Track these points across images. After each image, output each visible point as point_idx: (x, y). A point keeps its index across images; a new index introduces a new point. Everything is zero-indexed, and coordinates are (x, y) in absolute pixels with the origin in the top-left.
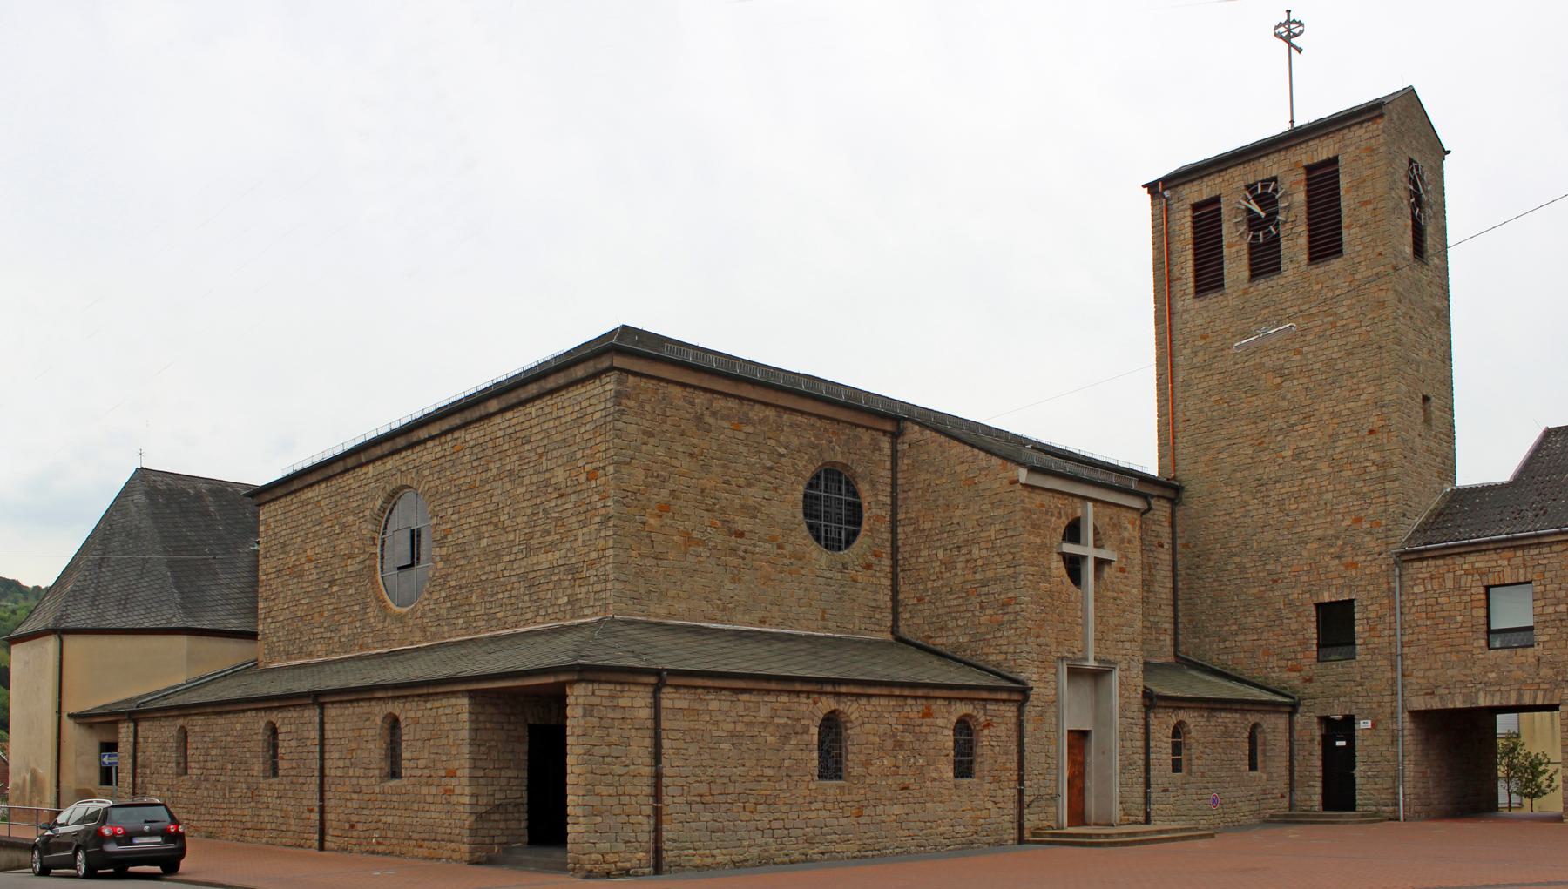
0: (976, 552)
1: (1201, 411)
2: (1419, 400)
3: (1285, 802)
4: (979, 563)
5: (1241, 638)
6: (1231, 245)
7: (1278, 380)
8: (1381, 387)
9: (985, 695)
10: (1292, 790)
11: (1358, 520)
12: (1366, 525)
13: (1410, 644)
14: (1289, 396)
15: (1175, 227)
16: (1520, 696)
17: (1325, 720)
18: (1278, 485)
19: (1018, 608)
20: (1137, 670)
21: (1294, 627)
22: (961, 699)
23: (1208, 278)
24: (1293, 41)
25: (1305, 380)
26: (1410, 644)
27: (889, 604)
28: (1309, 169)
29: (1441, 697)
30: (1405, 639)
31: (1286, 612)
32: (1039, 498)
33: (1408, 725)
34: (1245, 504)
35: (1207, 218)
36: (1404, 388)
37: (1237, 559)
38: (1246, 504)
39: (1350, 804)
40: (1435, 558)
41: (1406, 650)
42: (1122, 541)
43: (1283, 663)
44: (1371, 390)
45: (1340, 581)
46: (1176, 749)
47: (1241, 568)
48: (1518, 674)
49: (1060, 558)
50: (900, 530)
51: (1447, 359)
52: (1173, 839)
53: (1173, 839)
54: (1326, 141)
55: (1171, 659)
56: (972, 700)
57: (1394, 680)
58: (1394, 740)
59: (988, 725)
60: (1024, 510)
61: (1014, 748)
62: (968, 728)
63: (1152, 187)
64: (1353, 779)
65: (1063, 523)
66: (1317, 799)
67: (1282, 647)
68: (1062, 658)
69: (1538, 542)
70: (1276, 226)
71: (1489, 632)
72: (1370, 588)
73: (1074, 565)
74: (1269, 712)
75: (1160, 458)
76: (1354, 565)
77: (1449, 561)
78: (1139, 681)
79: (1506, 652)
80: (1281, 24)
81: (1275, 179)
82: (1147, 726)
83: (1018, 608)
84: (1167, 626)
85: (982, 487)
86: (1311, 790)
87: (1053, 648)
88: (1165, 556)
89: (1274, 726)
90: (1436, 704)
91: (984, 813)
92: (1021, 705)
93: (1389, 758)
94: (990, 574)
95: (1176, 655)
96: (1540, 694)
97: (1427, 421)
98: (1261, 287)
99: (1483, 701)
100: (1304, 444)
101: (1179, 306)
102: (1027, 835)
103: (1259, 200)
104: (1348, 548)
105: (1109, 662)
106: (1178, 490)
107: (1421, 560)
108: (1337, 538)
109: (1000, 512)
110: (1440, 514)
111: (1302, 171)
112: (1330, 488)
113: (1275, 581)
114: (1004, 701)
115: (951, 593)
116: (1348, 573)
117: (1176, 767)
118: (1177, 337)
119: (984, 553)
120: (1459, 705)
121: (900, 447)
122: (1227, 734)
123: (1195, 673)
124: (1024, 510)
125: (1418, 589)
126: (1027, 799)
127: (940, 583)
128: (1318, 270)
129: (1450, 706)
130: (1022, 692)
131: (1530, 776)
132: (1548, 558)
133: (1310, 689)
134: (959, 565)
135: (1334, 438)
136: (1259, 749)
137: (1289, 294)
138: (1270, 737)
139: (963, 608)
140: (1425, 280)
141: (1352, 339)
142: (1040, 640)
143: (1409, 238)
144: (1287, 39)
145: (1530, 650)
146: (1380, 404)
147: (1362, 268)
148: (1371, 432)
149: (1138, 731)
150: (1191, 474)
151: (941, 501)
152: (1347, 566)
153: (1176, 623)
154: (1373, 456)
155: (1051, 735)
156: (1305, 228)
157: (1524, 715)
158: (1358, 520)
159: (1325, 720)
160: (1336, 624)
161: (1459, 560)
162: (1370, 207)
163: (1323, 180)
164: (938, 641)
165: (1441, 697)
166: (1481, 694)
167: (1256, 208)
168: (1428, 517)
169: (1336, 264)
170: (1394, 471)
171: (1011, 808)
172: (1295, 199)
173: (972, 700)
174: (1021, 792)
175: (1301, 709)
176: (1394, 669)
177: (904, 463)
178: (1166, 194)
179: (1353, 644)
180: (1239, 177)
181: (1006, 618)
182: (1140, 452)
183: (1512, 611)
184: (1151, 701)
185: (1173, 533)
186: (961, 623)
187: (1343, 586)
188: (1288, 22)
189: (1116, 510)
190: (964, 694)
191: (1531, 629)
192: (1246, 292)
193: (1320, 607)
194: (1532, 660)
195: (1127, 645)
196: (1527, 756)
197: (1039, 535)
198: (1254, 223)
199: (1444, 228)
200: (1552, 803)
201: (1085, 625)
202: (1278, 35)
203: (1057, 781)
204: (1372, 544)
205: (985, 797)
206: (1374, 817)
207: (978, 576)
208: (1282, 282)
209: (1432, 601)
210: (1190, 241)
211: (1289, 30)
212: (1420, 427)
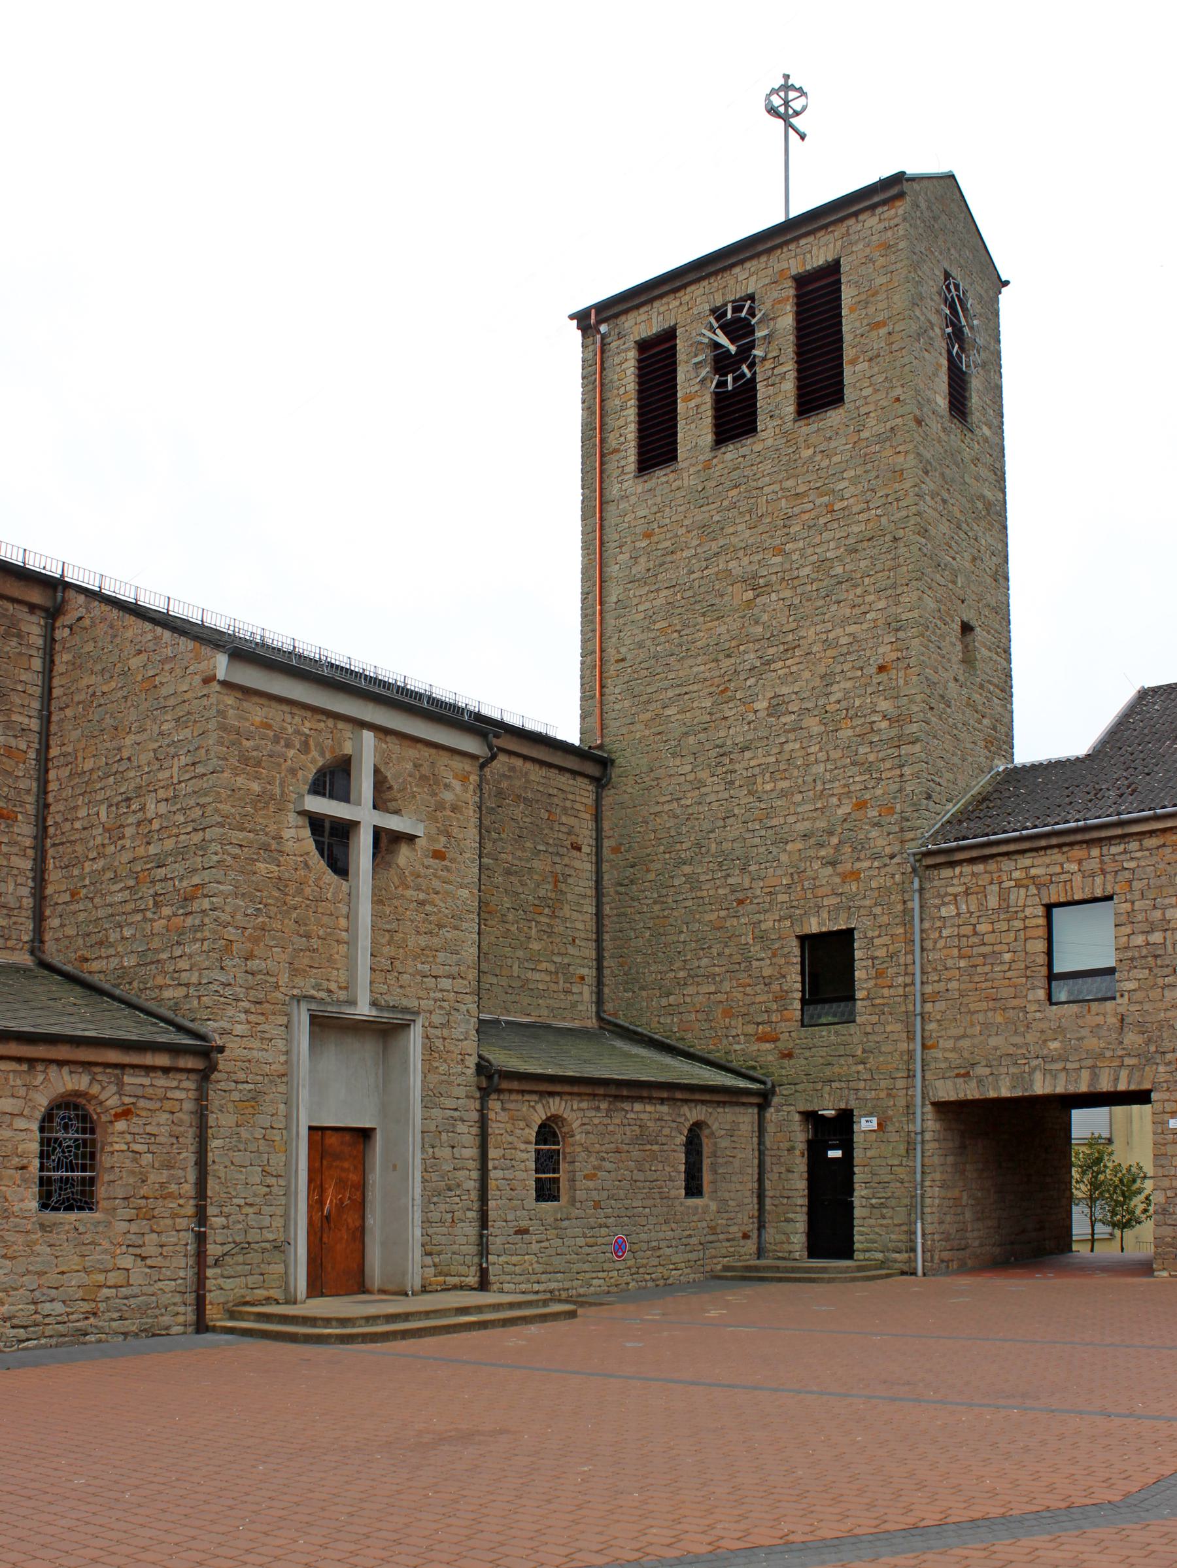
0: (151, 807)
1: (640, 645)
2: (957, 627)
3: (751, 1246)
4: (156, 825)
5: (691, 990)
6: (688, 398)
7: (750, 594)
8: (896, 600)
9: (114, 1056)
10: (761, 1227)
11: (861, 805)
12: (873, 813)
13: (935, 997)
14: (765, 617)
15: (612, 376)
16: (1094, 1077)
17: (810, 1117)
18: (748, 755)
19: (206, 904)
20: (464, 1028)
21: (767, 972)
22: (61, 1063)
23: (657, 447)
24: (793, 121)
25: (787, 593)
26: (935, 997)
27: (28, 902)
28: (801, 281)
29: (980, 1081)
30: (928, 989)
31: (756, 950)
32: (258, 713)
33: (930, 1124)
34: (699, 784)
35: (657, 359)
36: (931, 604)
37: (687, 869)
38: (702, 784)
39: (845, 1250)
40: (972, 861)
41: (929, 1007)
42: (440, 806)
43: (751, 1029)
44: (881, 604)
45: (833, 900)
46: (547, 1162)
47: (693, 882)
48: (1092, 1043)
49: (303, 821)
50: (52, 775)
51: (1001, 576)
52: (483, 1325)
53: (483, 1325)
54: (824, 238)
55: (592, 1023)
56: (87, 1065)
57: (911, 1054)
58: (910, 1149)
59: (126, 1113)
60: (223, 728)
61: (188, 1157)
62: (85, 1118)
63: (584, 320)
64: (850, 1207)
65: (314, 762)
66: (798, 1239)
67: (746, 1003)
68: (298, 999)
69: (1121, 833)
70: (751, 366)
71: (1051, 977)
72: (878, 910)
73: (333, 839)
74: (723, 1104)
75: (583, 717)
76: (855, 875)
77: (992, 866)
78: (470, 1046)
79: (1074, 1008)
80: (774, 91)
81: (752, 297)
82: (483, 1123)
83: (206, 904)
84: (585, 971)
85: (164, 691)
86: (788, 1227)
87: (284, 979)
88: (586, 866)
89: (730, 1128)
90: (970, 1091)
91: (113, 1278)
92: (205, 1076)
93: (906, 1179)
94: (169, 844)
95: (600, 1018)
96: (1124, 1074)
97: (968, 660)
98: (729, 456)
99: (1040, 1086)
100: (785, 690)
101: (614, 491)
102: (213, 1314)
103: (726, 328)
104: (847, 849)
105: (406, 1010)
106: (605, 763)
107: (952, 864)
108: (831, 833)
109: (187, 733)
110: (985, 799)
111: (789, 283)
112: (822, 756)
113: (741, 902)
114: (166, 1070)
115: (115, 879)
116: (846, 888)
117: (546, 1191)
118: (612, 536)
119: (163, 808)
120: (1005, 1093)
121: (58, 635)
122: (643, 1138)
123: (619, 1044)
124: (223, 728)
125: (948, 911)
126: (213, 1250)
127: (100, 864)
128: (806, 429)
129: (992, 1094)
130: (203, 1057)
131: (1118, 1197)
132: (1137, 857)
133: (791, 1068)
134: (129, 831)
135: (828, 679)
136: (706, 1162)
137: (767, 467)
138: (724, 1143)
139: (130, 907)
140: (967, 454)
141: (856, 529)
142: (253, 965)
143: (942, 383)
144: (785, 118)
145: (1109, 1005)
146: (895, 626)
147: (871, 422)
148: (882, 669)
149: (467, 1133)
150: (629, 747)
151: (109, 721)
152: (845, 877)
153: (600, 969)
154: (884, 705)
155: (276, 1136)
156: (796, 369)
157: (1119, 1110)
158: (861, 805)
159: (810, 1117)
160: (828, 967)
161: (1007, 864)
162: (883, 331)
163: (819, 297)
164: (95, 966)
165: (980, 1081)
166: (1038, 1076)
167: (723, 340)
168: (966, 806)
169: (834, 417)
170: (914, 728)
171: (181, 1267)
172: (779, 326)
173: (87, 1065)
174: (201, 1238)
175: (776, 1100)
176: (911, 1038)
177: (63, 659)
178: (603, 328)
179: (852, 998)
180: (703, 297)
181: (189, 921)
182: (554, 708)
183: (1086, 942)
184: (491, 1081)
185: (599, 830)
186: (127, 932)
187: (838, 908)
188: (786, 87)
189: (426, 752)
190: (63, 1052)
191: (1111, 971)
192: (707, 466)
193: (804, 939)
194: (1112, 1020)
195: (446, 983)
196: (1117, 1169)
197: (257, 778)
198: (722, 363)
199: (999, 388)
200: (1142, 1240)
201: (352, 943)
202: (772, 111)
203: (286, 1216)
204: (881, 842)
205: (121, 1249)
206: (881, 1271)
207: (153, 850)
208: (758, 447)
209: (967, 930)
210: (633, 394)
211: (786, 103)
212: (957, 668)
